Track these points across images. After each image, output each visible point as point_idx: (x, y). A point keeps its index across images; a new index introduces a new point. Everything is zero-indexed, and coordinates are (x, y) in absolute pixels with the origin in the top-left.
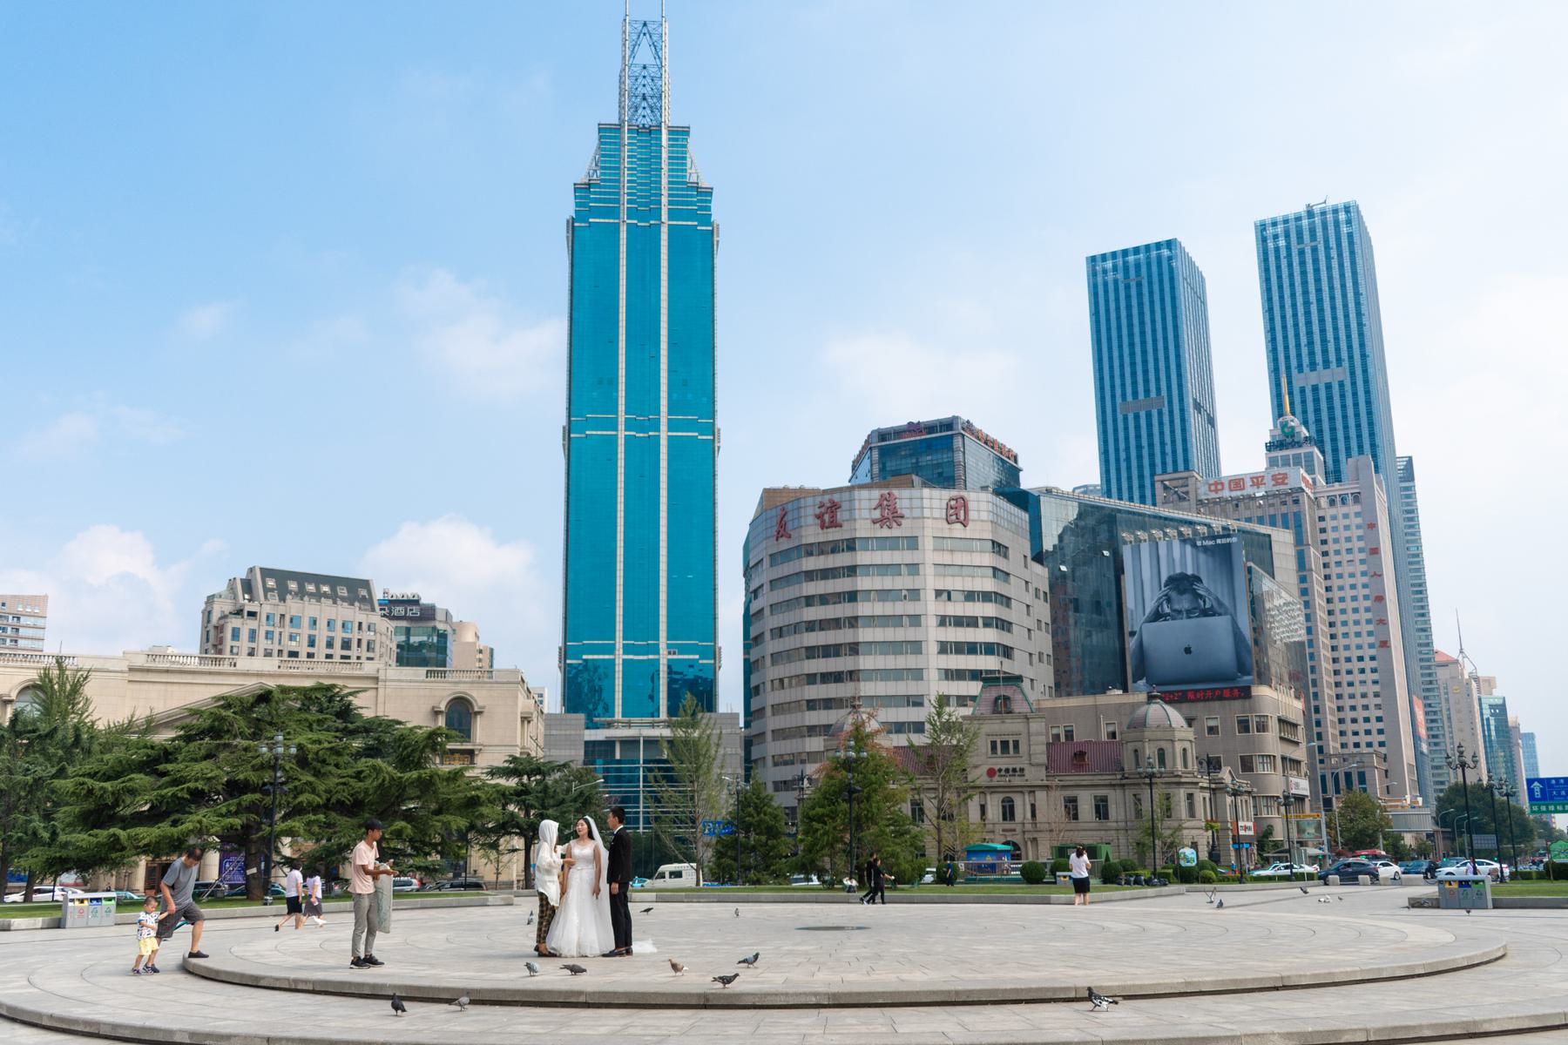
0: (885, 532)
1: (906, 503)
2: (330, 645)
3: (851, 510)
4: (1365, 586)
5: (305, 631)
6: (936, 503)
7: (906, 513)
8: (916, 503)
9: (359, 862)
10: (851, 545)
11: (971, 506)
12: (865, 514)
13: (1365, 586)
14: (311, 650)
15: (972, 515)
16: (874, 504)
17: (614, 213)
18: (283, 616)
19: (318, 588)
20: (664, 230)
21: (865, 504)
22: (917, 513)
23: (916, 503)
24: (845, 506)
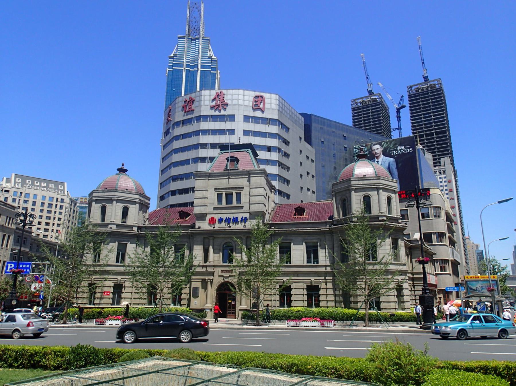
0: (217, 113)
1: (229, 97)
2: (43, 204)
3: (200, 101)
4: (446, 186)
5: (31, 200)
6: (246, 98)
7: (229, 102)
8: (235, 97)
9: (429, 263)
10: (199, 118)
11: (267, 101)
12: (207, 103)
13: (446, 186)
14: (33, 207)
15: (267, 106)
16: (212, 97)
17: (182, 65)
18: (21, 193)
19: (40, 184)
20: (199, 72)
21: (207, 98)
22: (235, 102)
23: (235, 97)
24: (197, 99)
